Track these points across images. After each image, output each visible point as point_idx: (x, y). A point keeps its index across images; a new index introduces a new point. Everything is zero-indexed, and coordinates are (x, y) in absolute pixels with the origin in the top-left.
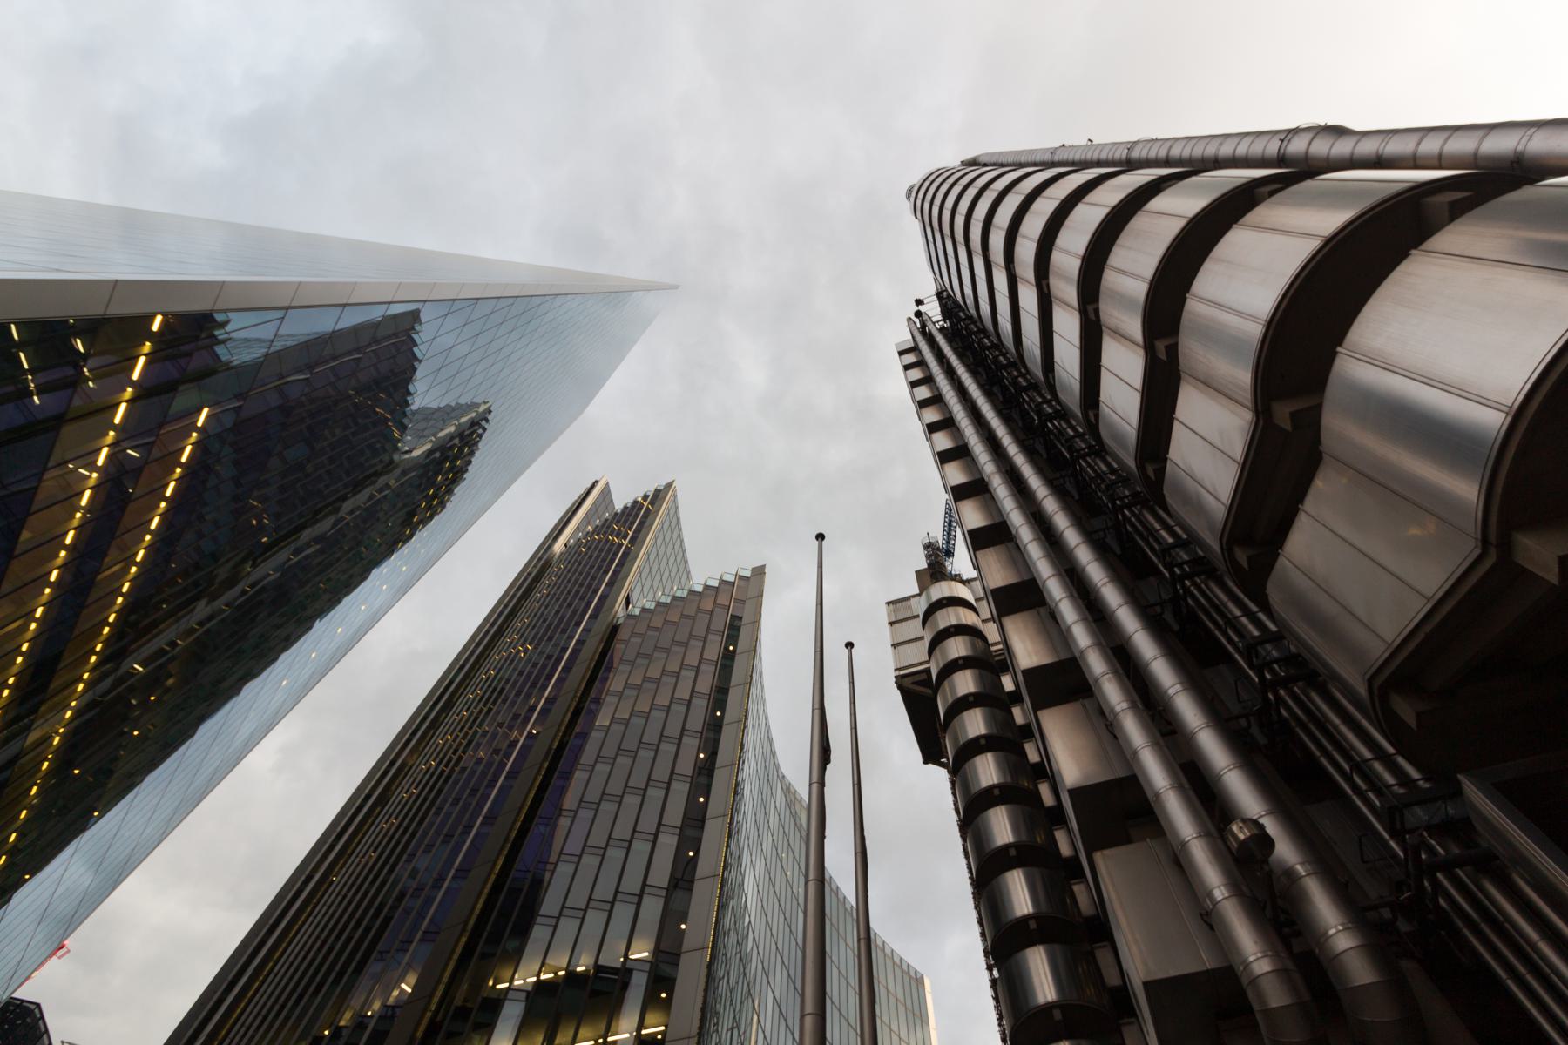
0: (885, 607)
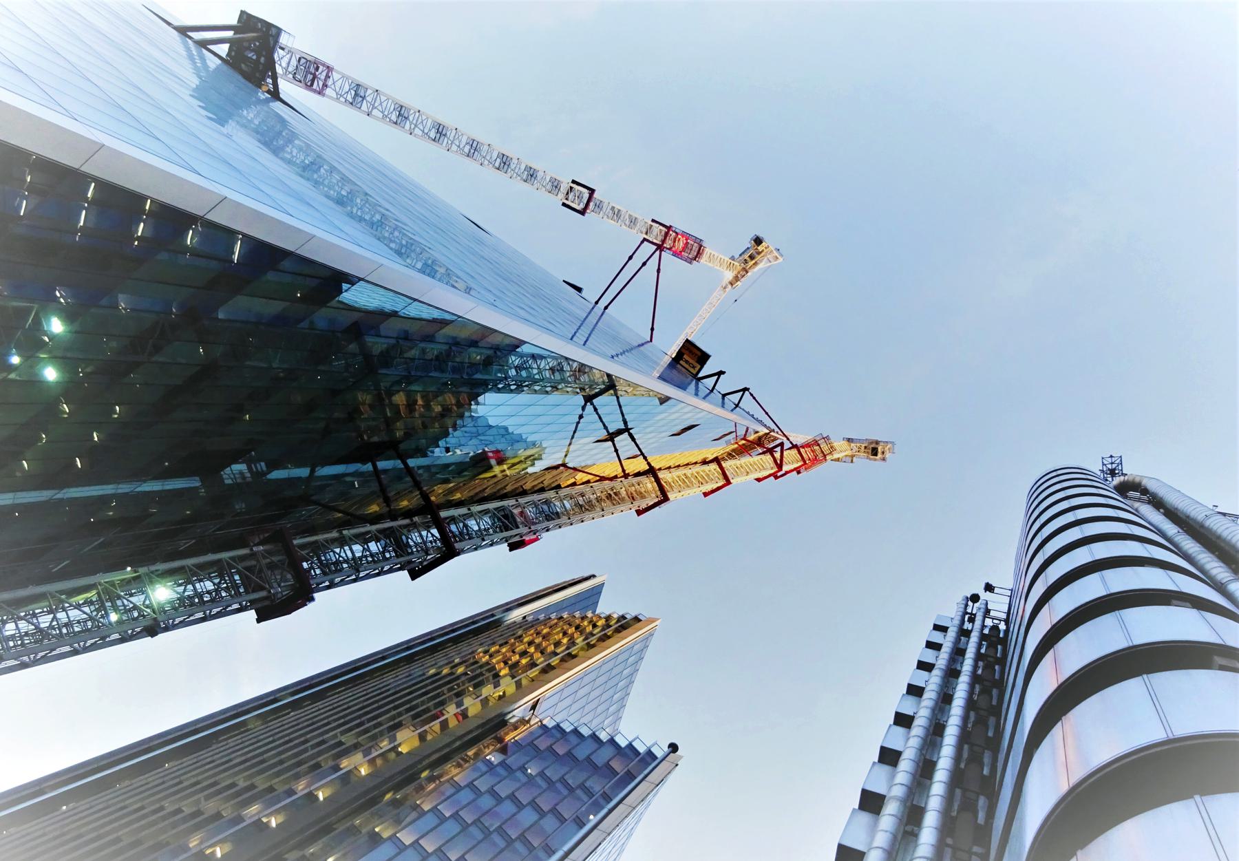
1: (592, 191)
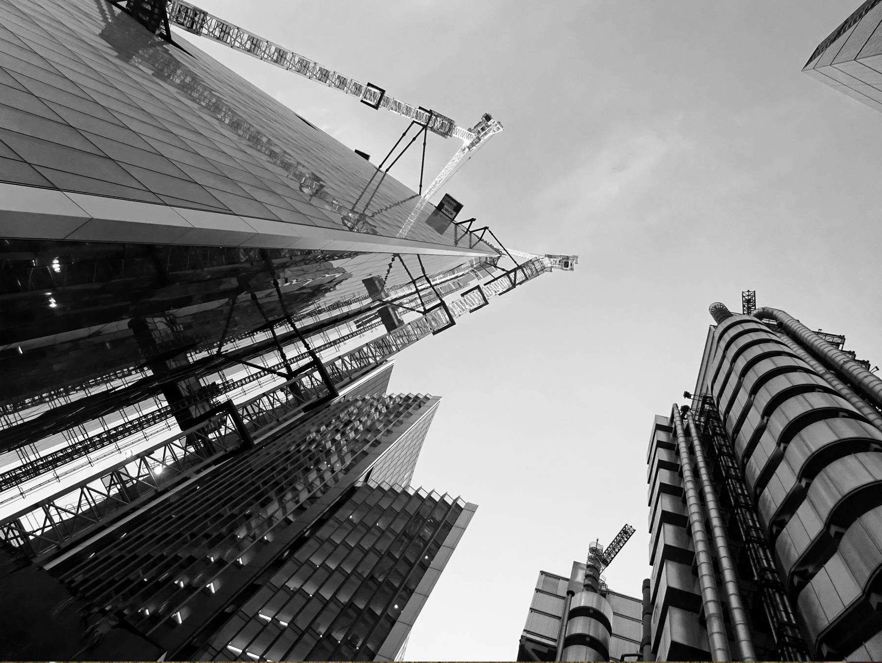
0: (539, 573)
1: (383, 92)
